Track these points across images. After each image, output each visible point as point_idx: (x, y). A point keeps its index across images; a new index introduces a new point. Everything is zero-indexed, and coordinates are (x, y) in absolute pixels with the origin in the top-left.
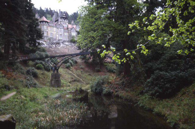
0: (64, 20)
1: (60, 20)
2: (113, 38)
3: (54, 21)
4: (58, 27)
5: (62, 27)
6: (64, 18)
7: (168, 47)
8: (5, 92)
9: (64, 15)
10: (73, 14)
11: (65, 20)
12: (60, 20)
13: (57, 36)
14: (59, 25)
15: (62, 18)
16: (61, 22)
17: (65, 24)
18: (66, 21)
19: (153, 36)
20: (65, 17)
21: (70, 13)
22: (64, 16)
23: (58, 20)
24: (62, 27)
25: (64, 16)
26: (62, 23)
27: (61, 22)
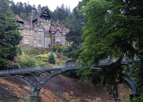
0: (44, 20)
1: (40, 20)
2: (87, 35)
3: (32, 22)
4: (36, 29)
5: (42, 30)
6: (44, 16)
7: (71, 60)
8: (25, 87)
9: (46, 12)
10: (49, 9)
11: (46, 19)
12: (40, 20)
13: (35, 42)
14: (38, 26)
15: (42, 16)
16: (41, 22)
17: (47, 25)
18: (47, 21)
19: (3, 41)
20: (46, 14)
21: (52, 9)
22: (46, 14)
23: (36, 20)
24: (42, 30)
25: (46, 14)
26: (42, 24)
27: (41, 22)
